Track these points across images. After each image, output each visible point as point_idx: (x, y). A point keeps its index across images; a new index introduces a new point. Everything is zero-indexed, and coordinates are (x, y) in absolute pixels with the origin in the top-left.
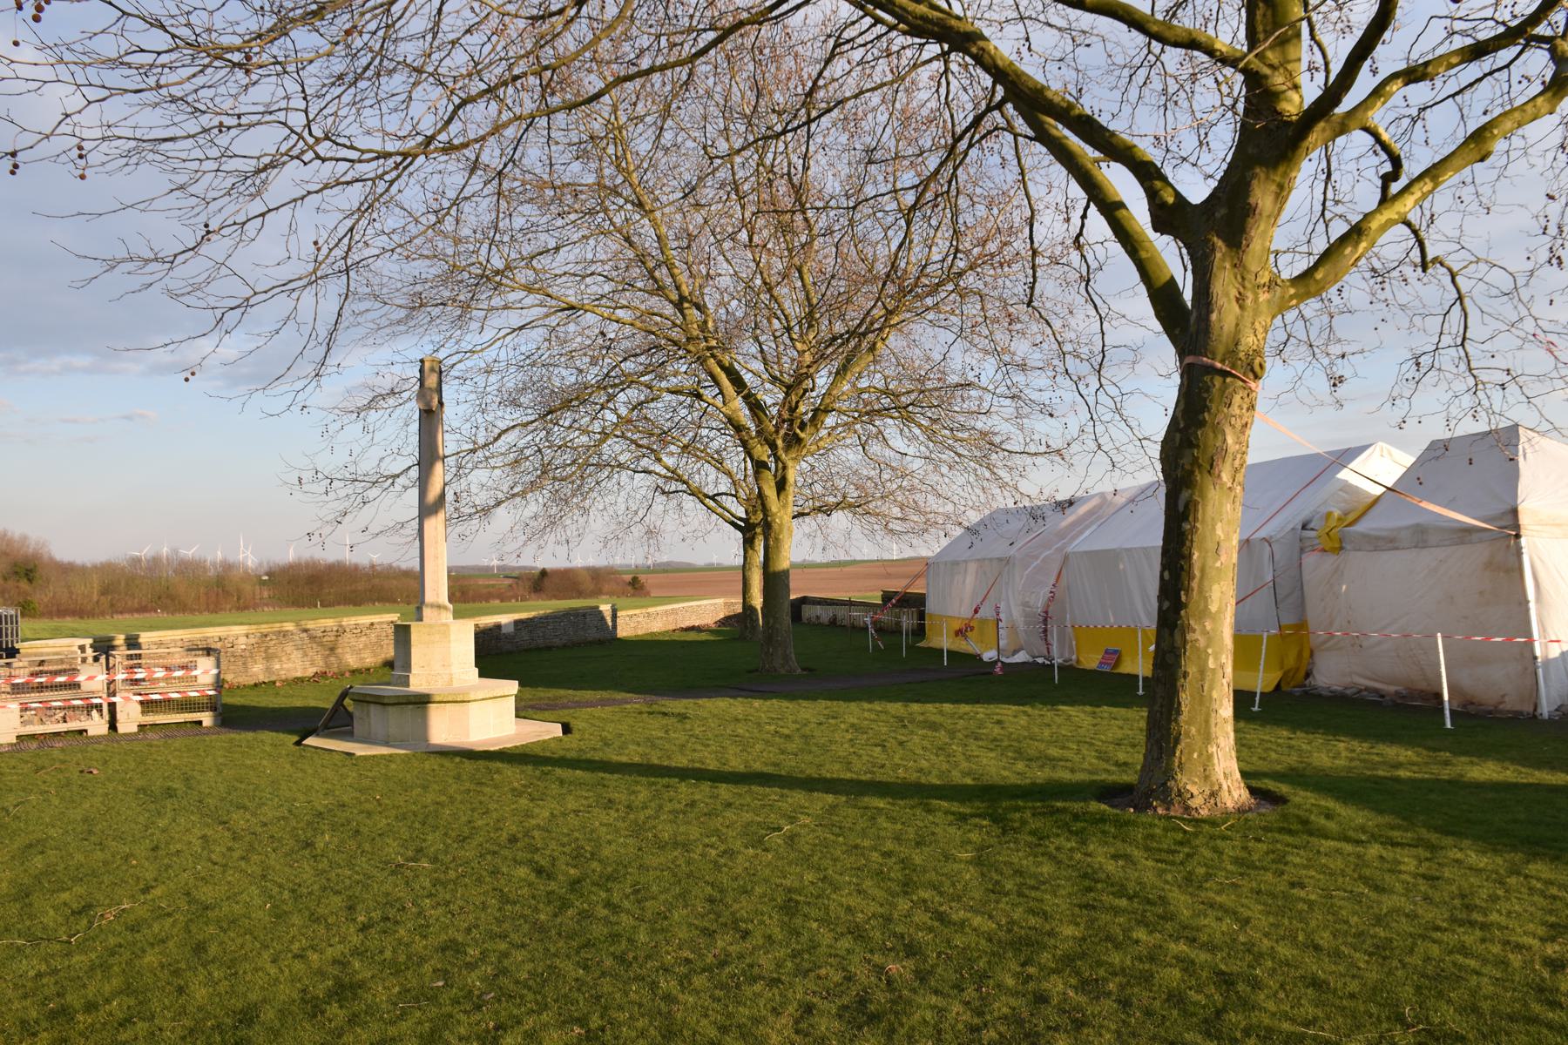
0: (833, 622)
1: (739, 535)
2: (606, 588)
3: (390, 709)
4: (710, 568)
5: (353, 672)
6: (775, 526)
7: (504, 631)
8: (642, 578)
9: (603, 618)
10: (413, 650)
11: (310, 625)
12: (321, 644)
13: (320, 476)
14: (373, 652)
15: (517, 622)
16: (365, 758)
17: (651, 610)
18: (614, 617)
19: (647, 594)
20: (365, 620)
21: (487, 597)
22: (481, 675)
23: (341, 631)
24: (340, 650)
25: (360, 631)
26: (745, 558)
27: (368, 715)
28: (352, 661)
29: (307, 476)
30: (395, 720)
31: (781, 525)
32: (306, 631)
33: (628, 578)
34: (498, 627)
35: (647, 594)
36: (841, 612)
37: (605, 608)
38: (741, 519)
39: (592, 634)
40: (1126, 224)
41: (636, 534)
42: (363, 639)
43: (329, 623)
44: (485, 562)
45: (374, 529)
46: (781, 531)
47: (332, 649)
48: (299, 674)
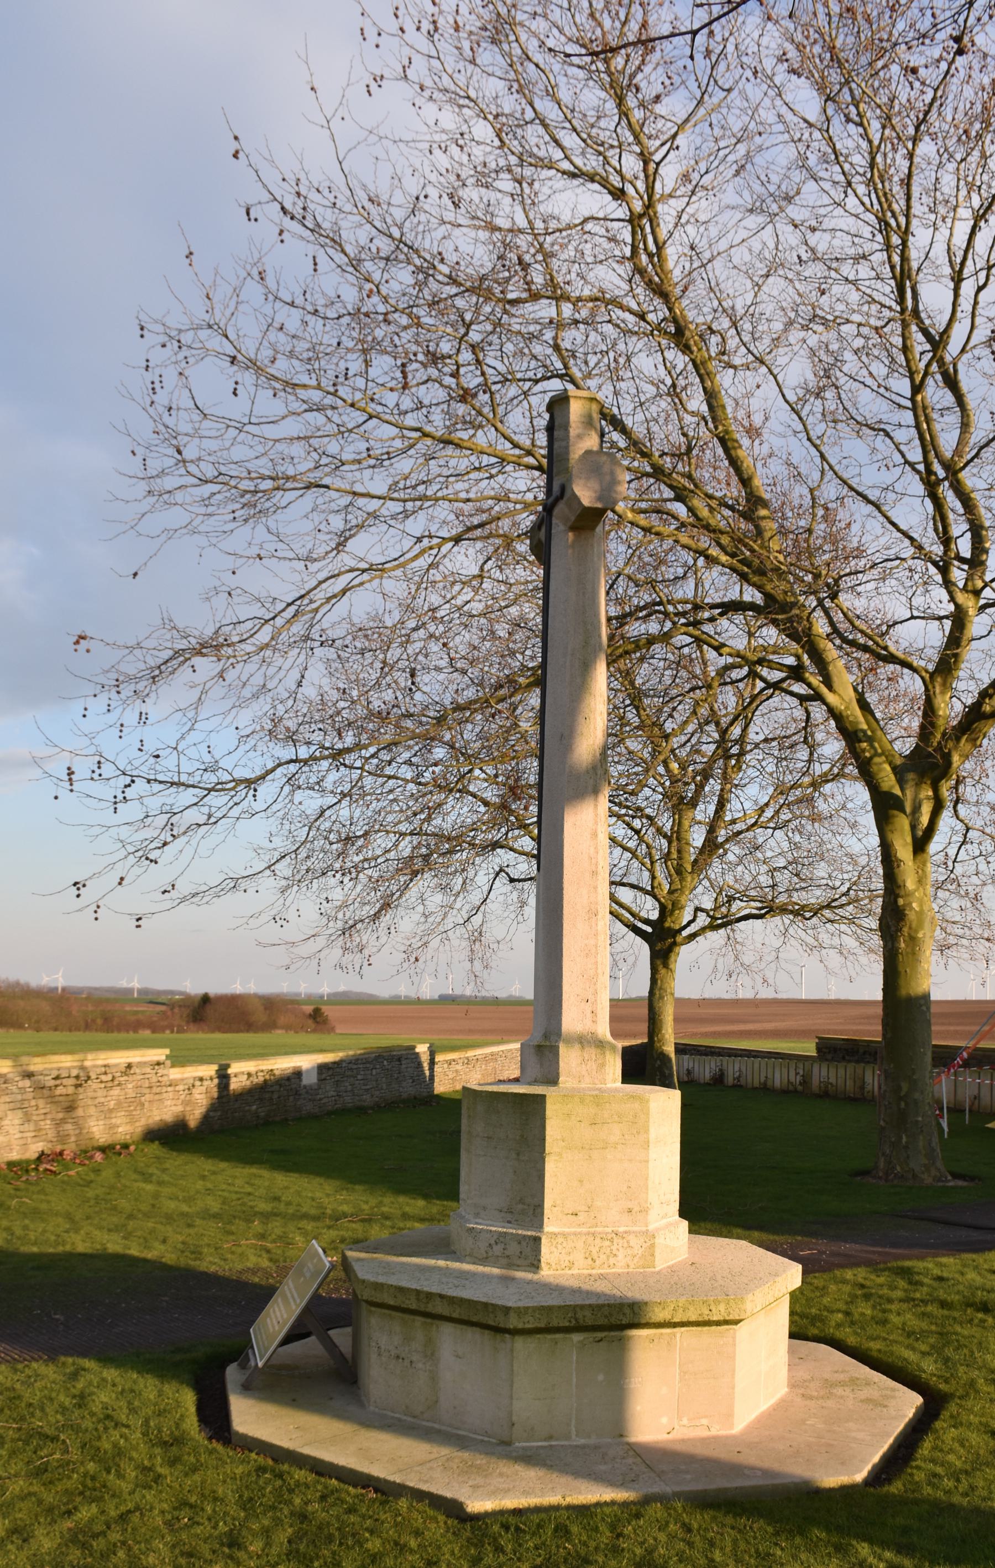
0: (719, 1079)
1: (645, 949)
2: (282, 1020)
3: (520, 1343)
4: (395, 1001)
5: (103, 1149)
6: (911, 916)
7: (306, 1081)
8: (324, 1008)
9: (420, 1065)
10: (551, 1167)
11: (37, 1064)
12: (52, 1099)
13: (108, 770)
14: (130, 1115)
15: (322, 1068)
16: (515, 1521)
17: (470, 1053)
18: (432, 1063)
19: (332, 1030)
20: (118, 1058)
21: (136, 1026)
22: (690, 1232)
23: (82, 1080)
24: (80, 1112)
25: (111, 1078)
26: (654, 980)
27: (430, 1352)
28: (98, 1131)
29: (83, 768)
30: (536, 1382)
31: (920, 914)
32: (29, 1075)
33: (309, 1009)
34: (298, 1073)
35: (332, 1030)
36: (733, 1069)
37: (422, 1049)
38: (647, 922)
39: (408, 1089)
40: (581, 719)
41: (455, 942)
42: (116, 1091)
43: (66, 1062)
44: (124, 984)
45: (184, 888)
46: (921, 925)
47: (70, 1108)
48: (15, 1156)
